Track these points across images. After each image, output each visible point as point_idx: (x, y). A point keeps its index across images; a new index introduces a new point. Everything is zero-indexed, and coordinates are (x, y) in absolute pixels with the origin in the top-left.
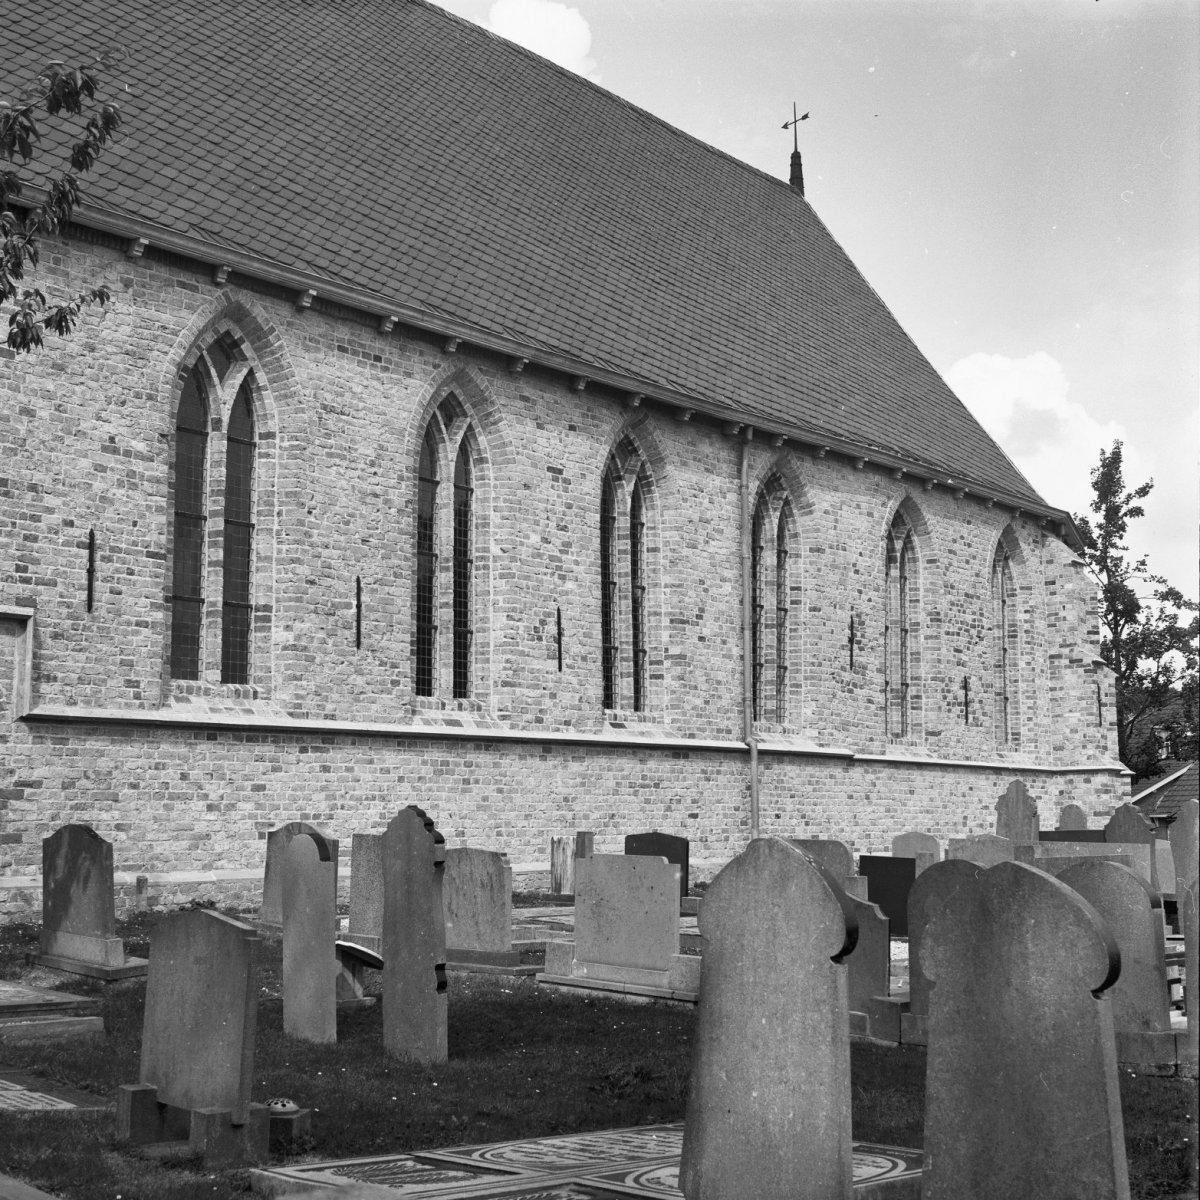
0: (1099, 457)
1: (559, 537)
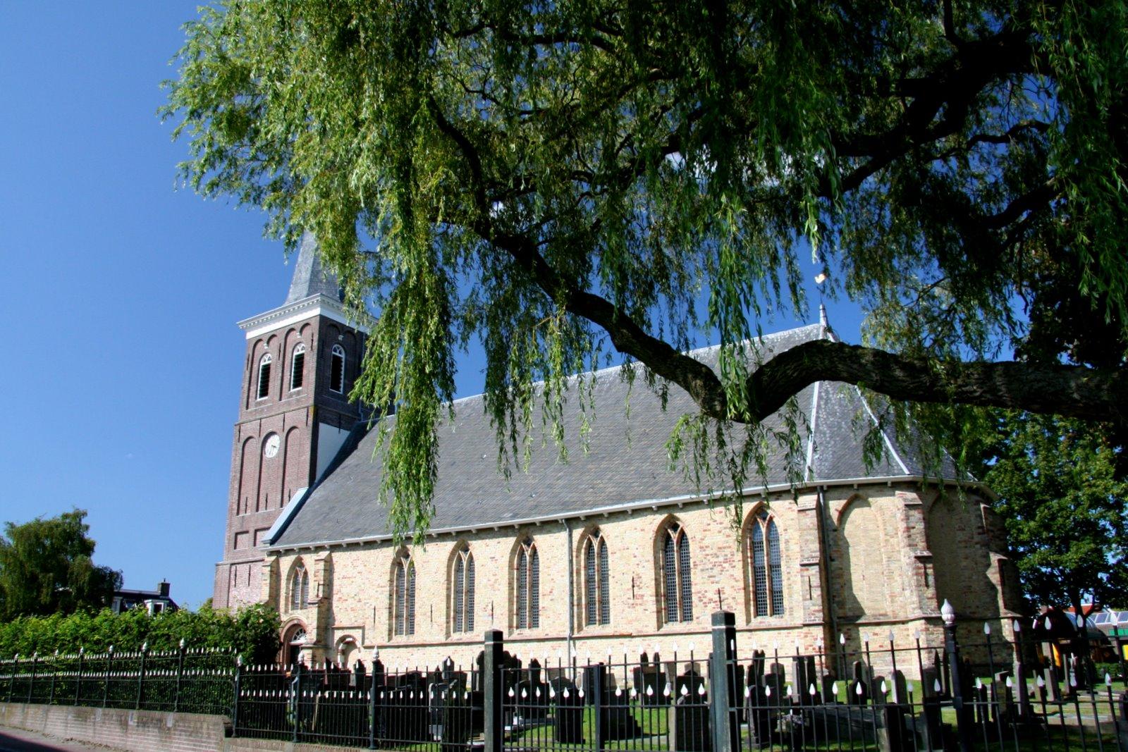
1: (493, 579)
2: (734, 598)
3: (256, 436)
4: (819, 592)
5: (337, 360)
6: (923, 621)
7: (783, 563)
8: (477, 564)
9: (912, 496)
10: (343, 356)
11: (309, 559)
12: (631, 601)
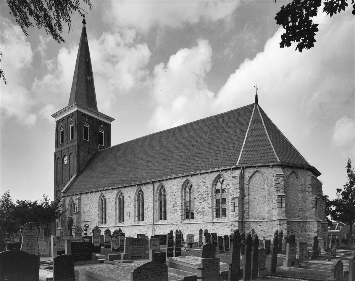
0: (347, 174)
1: (129, 204)
2: (208, 211)
3: (67, 154)
5: (86, 129)
6: (278, 221)
8: (125, 199)
9: (280, 171)
10: (89, 127)
11: (74, 198)
12: (173, 212)
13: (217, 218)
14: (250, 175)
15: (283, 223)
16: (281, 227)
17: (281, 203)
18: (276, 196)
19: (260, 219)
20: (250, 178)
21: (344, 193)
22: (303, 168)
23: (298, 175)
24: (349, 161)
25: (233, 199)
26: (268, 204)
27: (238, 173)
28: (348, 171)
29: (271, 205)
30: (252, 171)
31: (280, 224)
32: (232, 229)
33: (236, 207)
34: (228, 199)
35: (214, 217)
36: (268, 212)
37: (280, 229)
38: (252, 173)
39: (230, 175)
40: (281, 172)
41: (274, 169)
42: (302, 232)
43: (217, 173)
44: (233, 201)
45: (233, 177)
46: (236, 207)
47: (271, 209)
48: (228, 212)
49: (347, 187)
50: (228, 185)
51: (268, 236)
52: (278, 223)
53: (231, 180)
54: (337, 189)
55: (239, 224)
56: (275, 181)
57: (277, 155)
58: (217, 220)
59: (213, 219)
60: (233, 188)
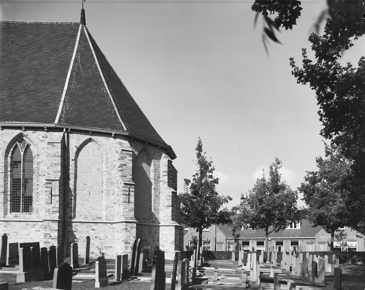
0: (196, 159)
4: (57, 198)
6: (124, 223)
7: (34, 177)
13: (14, 214)
14: (78, 144)
15: (131, 227)
16: (128, 234)
17: (128, 196)
18: (121, 184)
19: (94, 219)
20: (79, 149)
21: (193, 187)
22: (157, 146)
23: (150, 155)
24: (200, 142)
25: (50, 181)
26: (107, 195)
27: (57, 136)
28: (199, 155)
29: (112, 197)
30: (84, 138)
31: (126, 229)
32: (48, 234)
33: (55, 196)
34: (38, 181)
35: (9, 212)
36: (106, 209)
37: (126, 237)
38: (81, 142)
39: (43, 139)
40: (129, 147)
41: (118, 140)
42: (153, 241)
43: (18, 132)
44: (49, 185)
45: (49, 143)
46: (55, 196)
47: (112, 204)
48: (37, 203)
49: (196, 177)
50: (39, 155)
51: (106, 247)
52: (124, 227)
53: (44, 148)
54: (185, 180)
55: (59, 226)
56: (119, 159)
57: (122, 119)
58: (14, 216)
59: (5, 214)
60: (49, 163)
